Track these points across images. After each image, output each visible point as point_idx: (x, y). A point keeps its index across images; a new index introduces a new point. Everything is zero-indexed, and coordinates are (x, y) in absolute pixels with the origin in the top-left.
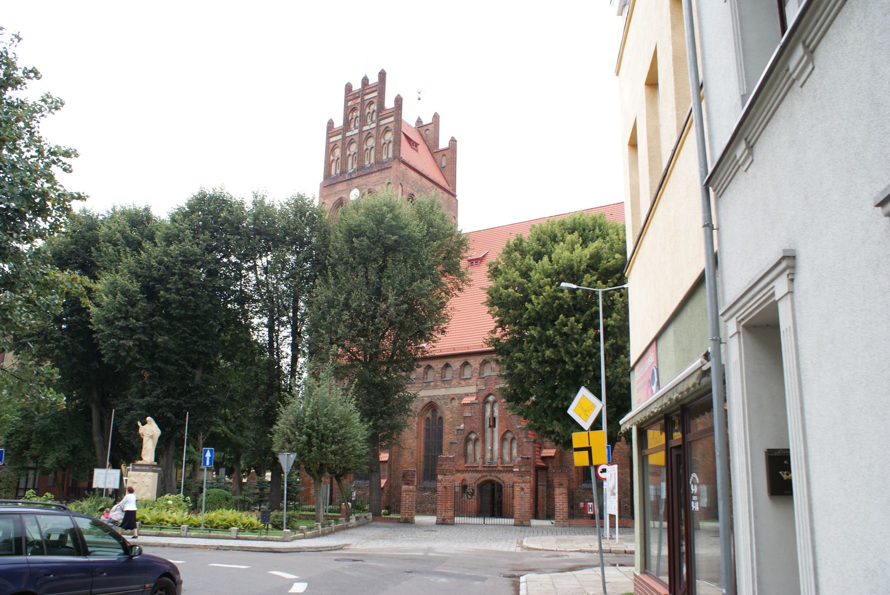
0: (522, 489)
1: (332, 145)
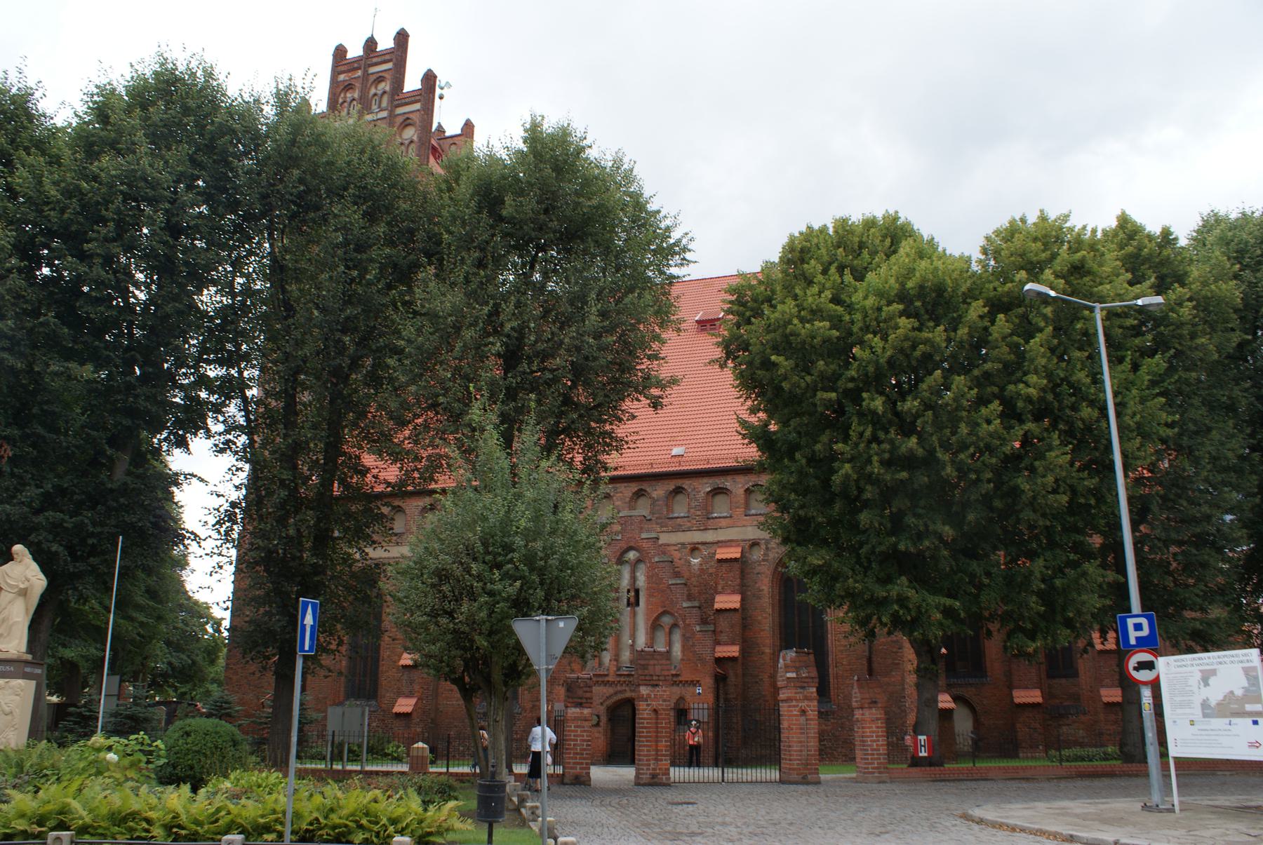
0: (803, 712)
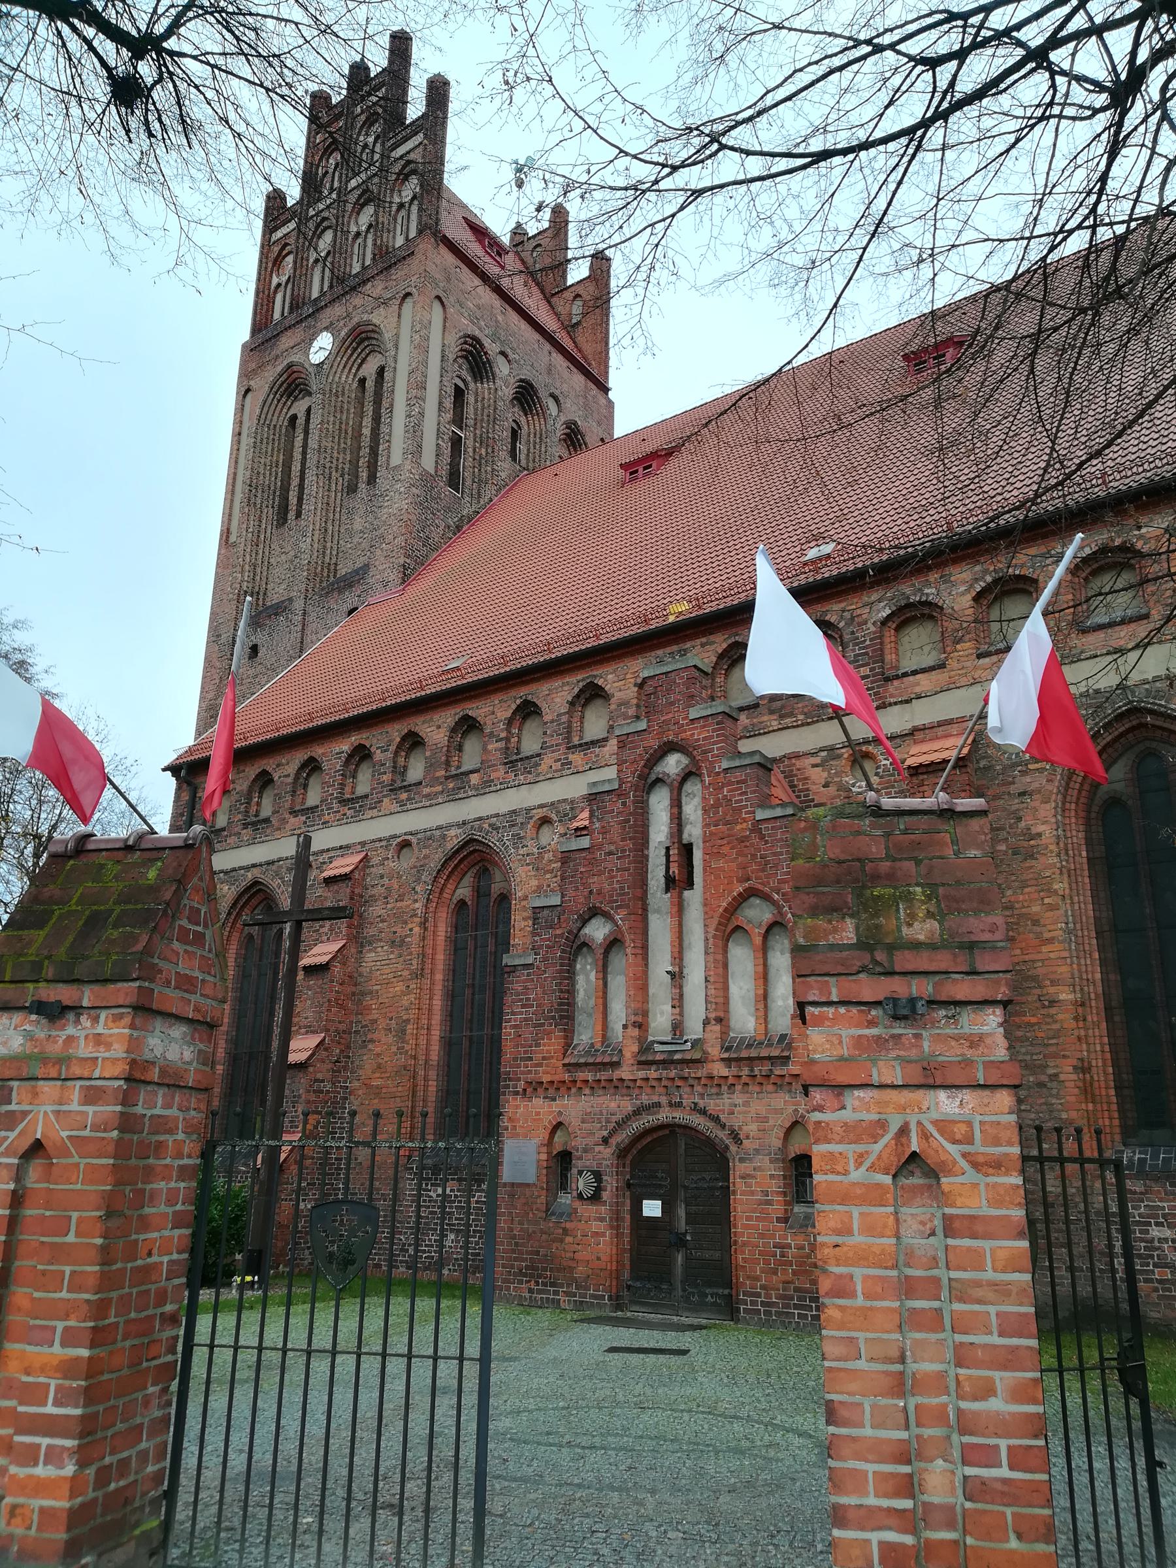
1: (276, 249)
